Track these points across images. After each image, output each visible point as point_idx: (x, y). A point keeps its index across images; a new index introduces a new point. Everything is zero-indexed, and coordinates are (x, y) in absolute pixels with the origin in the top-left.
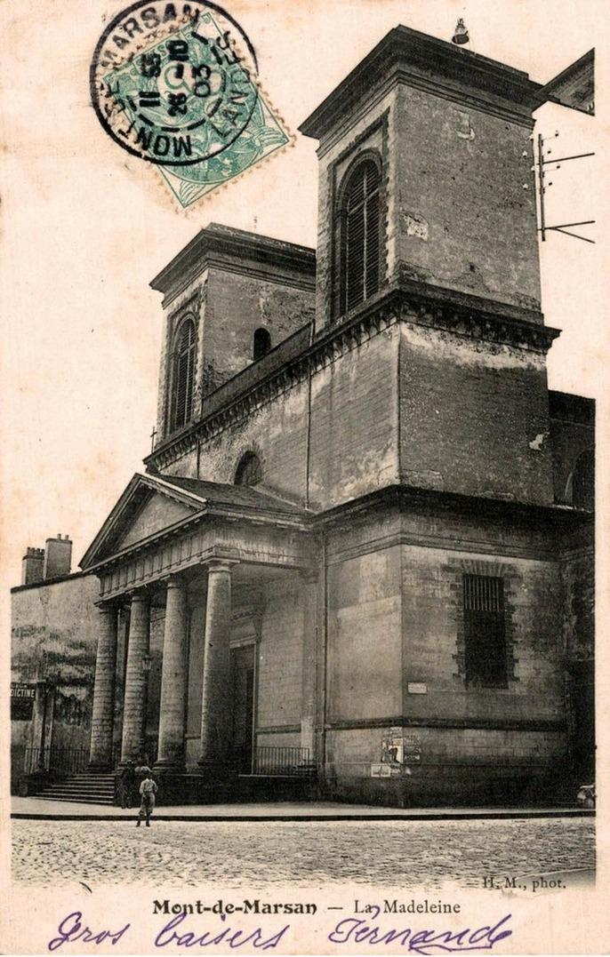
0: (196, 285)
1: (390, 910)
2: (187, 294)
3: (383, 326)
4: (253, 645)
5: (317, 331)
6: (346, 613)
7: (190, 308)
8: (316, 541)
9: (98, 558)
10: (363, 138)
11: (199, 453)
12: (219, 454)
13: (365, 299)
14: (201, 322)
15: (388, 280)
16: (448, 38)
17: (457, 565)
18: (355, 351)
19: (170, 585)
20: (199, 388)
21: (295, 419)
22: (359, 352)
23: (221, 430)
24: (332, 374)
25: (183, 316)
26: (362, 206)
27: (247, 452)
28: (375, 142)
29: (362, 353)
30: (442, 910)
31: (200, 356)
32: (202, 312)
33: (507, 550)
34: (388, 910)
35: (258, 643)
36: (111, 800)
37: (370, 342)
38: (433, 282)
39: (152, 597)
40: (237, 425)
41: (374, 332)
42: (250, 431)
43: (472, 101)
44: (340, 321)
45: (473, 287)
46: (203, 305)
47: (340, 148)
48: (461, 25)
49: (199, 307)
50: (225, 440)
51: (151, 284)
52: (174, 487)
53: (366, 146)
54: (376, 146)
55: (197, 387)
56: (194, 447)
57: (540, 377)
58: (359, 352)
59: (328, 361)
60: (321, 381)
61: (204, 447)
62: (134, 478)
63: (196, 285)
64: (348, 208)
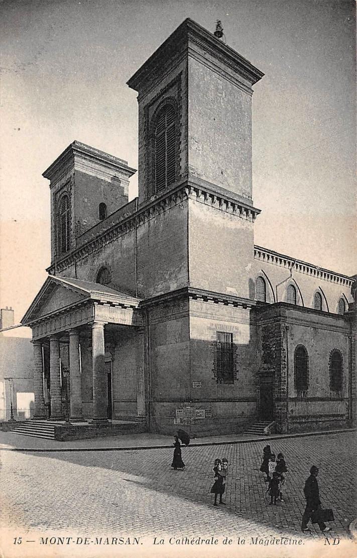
0: (68, 176)
1: (43, 543)
2: (64, 181)
3: (179, 201)
4: (110, 362)
5: (140, 203)
6: (161, 349)
7: (65, 189)
8: (143, 314)
9: (31, 318)
10: (165, 91)
11: (76, 267)
12: (88, 266)
13: (166, 186)
14: (73, 196)
15: (181, 175)
16: (212, 32)
17: (214, 327)
18: (162, 215)
19: (51, 340)
20: (73, 233)
21: (128, 250)
22: (164, 214)
23: (87, 255)
24: (149, 226)
25: (62, 193)
26: (164, 133)
27: (102, 267)
28: (173, 93)
29: (166, 215)
30: (110, 542)
31: (73, 215)
32: (72, 191)
33: (236, 319)
34: (42, 543)
35: (113, 361)
36: (53, 431)
37: (171, 210)
38: (204, 178)
39: (62, 337)
40: (96, 252)
41: (173, 204)
42: (103, 255)
43: (224, 74)
44: (153, 199)
45: (222, 183)
46: (73, 187)
47: (151, 96)
48: (218, 26)
49: (71, 189)
50: (90, 261)
51: (43, 175)
52: (71, 284)
53: (166, 96)
54: (173, 95)
55: (72, 232)
56: (73, 263)
57: (251, 235)
58: (164, 214)
59: (146, 220)
60: (142, 230)
61: (78, 264)
62: (48, 279)
63: (68, 176)
64: (156, 133)
